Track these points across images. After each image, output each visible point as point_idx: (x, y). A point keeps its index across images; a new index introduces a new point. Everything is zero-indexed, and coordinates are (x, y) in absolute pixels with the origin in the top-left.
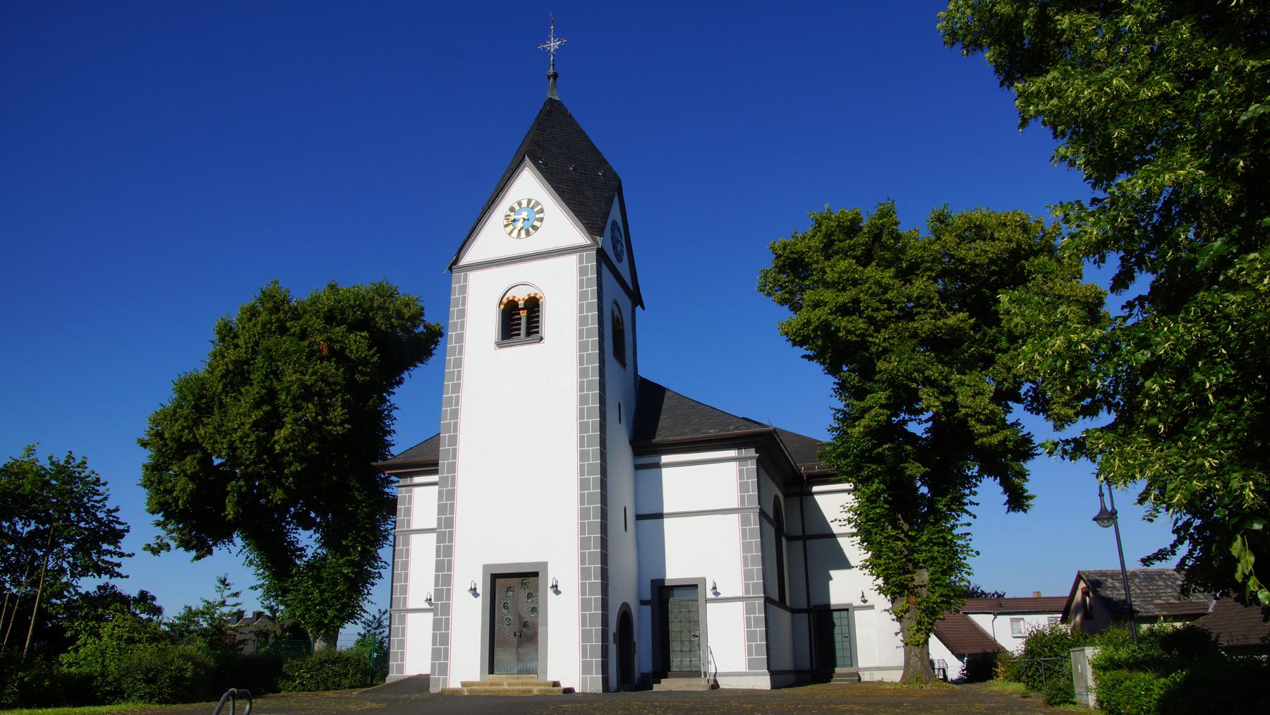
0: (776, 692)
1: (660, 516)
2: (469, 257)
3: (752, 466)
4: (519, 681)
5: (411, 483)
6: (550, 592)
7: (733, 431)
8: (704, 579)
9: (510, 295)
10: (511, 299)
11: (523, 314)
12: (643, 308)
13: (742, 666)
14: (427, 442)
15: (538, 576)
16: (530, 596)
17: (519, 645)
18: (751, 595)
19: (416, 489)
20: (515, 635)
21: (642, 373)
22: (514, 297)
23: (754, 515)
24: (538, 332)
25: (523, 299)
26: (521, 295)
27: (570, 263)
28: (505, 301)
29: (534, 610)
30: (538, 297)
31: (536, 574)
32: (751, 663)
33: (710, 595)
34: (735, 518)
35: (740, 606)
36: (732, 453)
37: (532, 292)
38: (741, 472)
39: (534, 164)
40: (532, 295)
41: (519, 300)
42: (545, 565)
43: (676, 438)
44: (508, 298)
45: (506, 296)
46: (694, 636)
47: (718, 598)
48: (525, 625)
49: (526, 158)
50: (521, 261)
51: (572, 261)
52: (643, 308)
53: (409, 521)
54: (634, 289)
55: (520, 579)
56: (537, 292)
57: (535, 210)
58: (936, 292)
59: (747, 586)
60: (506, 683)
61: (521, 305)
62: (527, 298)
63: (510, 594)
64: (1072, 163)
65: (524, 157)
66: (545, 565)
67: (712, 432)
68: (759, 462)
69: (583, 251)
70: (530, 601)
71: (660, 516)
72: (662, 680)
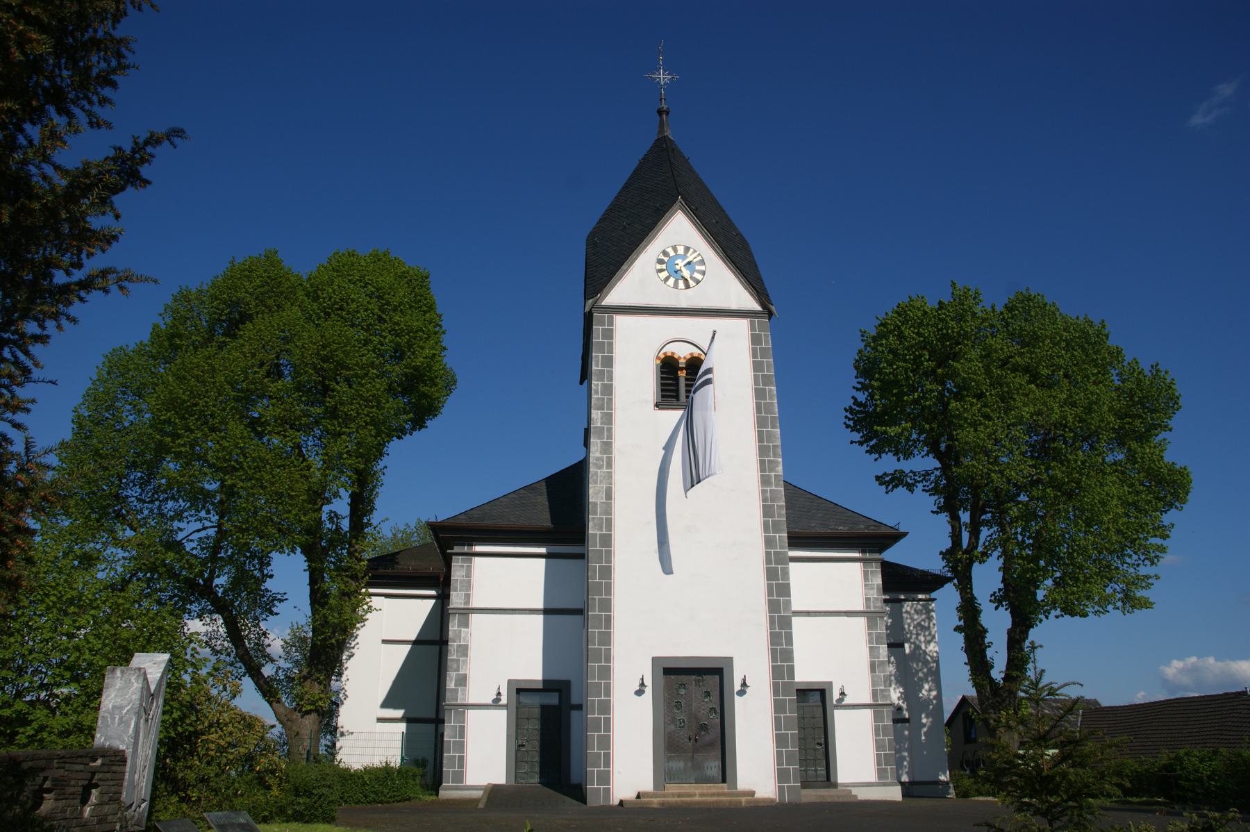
0: (910, 801)
1: (546, 611)
2: (618, 294)
4: (714, 791)
5: (469, 551)
7: (861, 528)
8: (831, 683)
9: (669, 349)
10: (669, 354)
11: (682, 374)
13: (871, 775)
14: (492, 503)
17: (696, 750)
19: (477, 560)
20: (690, 739)
22: (673, 353)
25: (685, 358)
26: (683, 352)
32: (881, 773)
41: (680, 358)
42: (729, 660)
44: (665, 354)
45: (662, 352)
47: (840, 705)
50: (681, 315)
51: (743, 324)
58: (402, 375)
60: (811, 795)
61: (682, 363)
62: (689, 357)
64: (898, 307)
66: (729, 660)
69: (757, 317)
71: (546, 611)
72: (853, 794)
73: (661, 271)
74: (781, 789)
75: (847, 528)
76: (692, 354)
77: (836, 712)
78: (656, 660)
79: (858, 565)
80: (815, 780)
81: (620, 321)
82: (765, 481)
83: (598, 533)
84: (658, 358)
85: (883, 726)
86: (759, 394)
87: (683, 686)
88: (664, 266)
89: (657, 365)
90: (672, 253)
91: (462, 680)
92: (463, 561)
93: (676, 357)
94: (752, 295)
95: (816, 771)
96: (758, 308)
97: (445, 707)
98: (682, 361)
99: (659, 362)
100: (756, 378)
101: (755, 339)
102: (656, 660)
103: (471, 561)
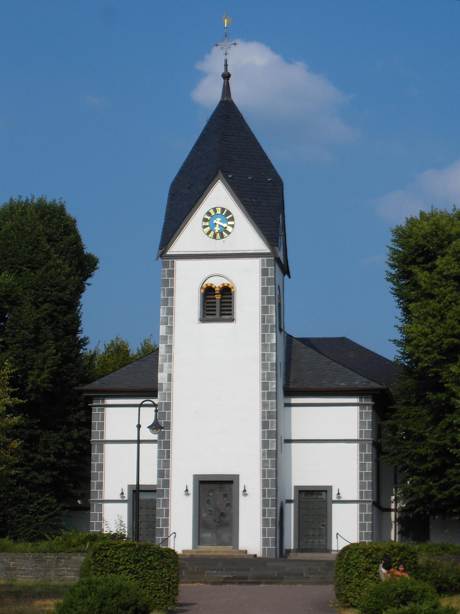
3: (369, 410)
5: (103, 404)
6: (191, 491)
8: (331, 487)
9: (209, 282)
10: (209, 285)
12: (290, 277)
15: (233, 483)
16: (225, 495)
18: (364, 499)
21: (290, 329)
22: (212, 284)
23: (368, 445)
24: (230, 314)
25: (219, 287)
26: (217, 283)
27: (256, 263)
28: (204, 286)
29: (228, 505)
30: (230, 287)
31: (231, 482)
33: (334, 498)
34: (355, 446)
35: (356, 507)
36: (355, 400)
37: (226, 282)
38: (361, 414)
39: (225, 177)
40: (226, 285)
41: (216, 287)
42: (238, 476)
43: (316, 387)
44: (207, 285)
46: (322, 525)
48: (222, 514)
49: (220, 173)
51: (256, 263)
52: (290, 277)
53: (102, 433)
54: (284, 262)
55: (218, 486)
56: (229, 283)
57: (227, 218)
59: (361, 493)
62: (221, 286)
63: (211, 494)
65: (218, 172)
67: (343, 385)
68: (374, 408)
70: (225, 499)
73: (205, 227)
74: (264, 550)
75: (346, 384)
76: (223, 284)
77: (334, 506)
78: (196, 477)
79: (356, 409)
80: (318, 547)
81: (179, 264)
82: (264, 367)
83: (163, 402)
84: (202, 288)
85: (162, 519)
86: (264, 310)
87: (211, 490)
88: (207, 224)
89: (201, 293)
90: (213, 214)
91: (100, 485)
92: (99, 410)
93: (213, 287)
94: (264, 241)
95: (320, 542)
96: (268, 251)
97: (90, 502)
98: (217, 289)
99: (203, 291)
100: (263, 299)
101: (264, 272)
102: (196, 477)
103: (103, 410)
